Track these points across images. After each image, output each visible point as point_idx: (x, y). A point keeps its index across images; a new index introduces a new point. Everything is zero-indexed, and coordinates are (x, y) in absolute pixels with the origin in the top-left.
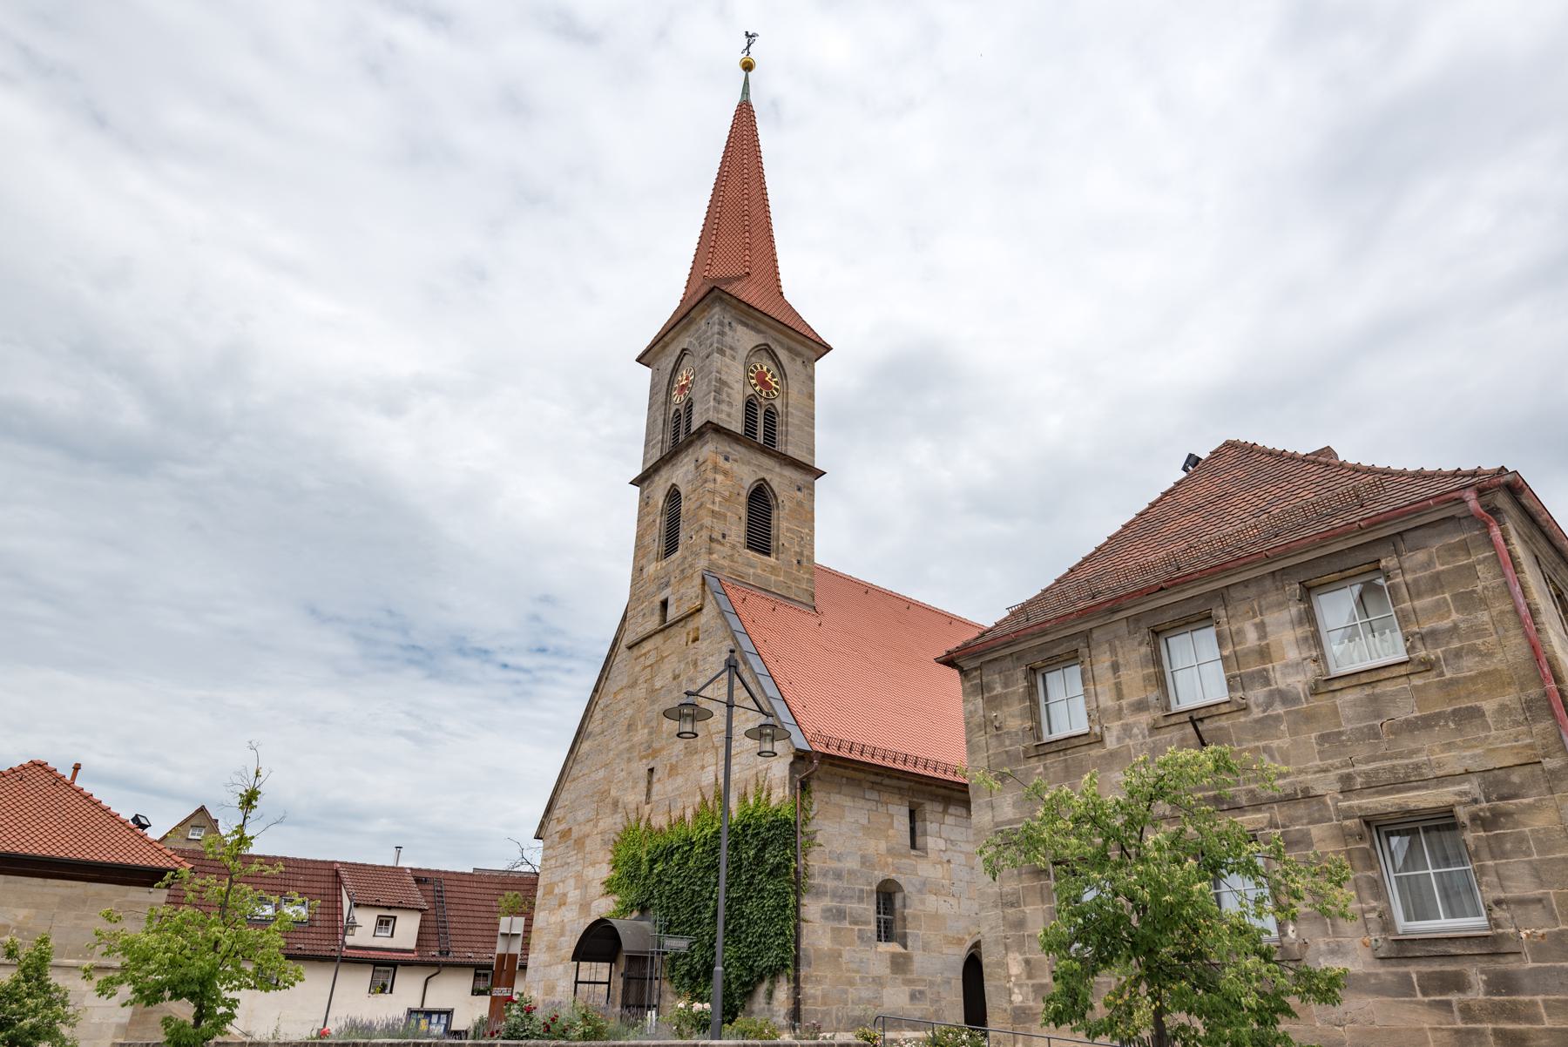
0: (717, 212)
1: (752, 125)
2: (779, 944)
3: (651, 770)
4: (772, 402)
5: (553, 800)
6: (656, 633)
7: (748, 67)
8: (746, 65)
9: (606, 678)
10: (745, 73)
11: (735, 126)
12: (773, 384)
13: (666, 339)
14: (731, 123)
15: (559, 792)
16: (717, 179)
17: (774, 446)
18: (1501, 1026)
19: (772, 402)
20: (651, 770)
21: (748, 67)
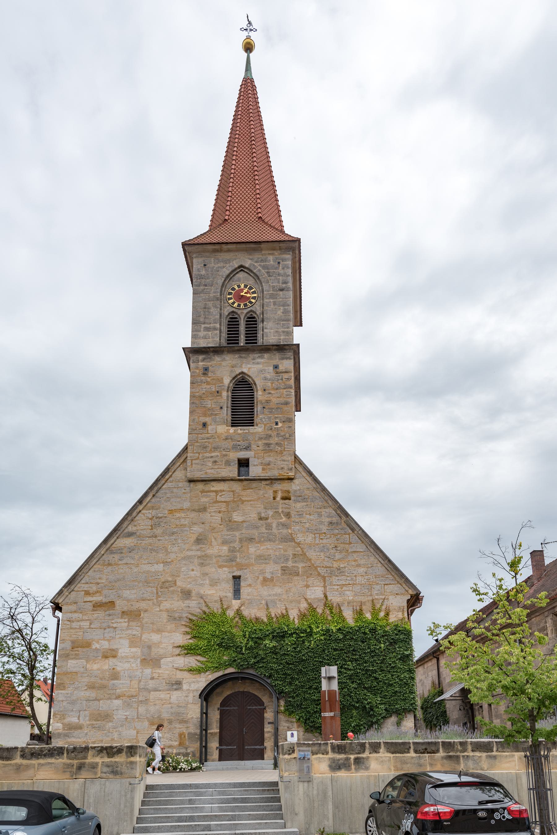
0: (227, 210)
1: (254, 94)
2: (290, 701)
3: (237, 579)
4: (251, 308)
5: (74, 578)
6: (232, 480)
7: (249, 48)
8: (248, 46)
9: (154, 496)
10: (246, 54)
11: (241, 101)
12: (248, 295)
13: (224, 246)
14: (238, 96)
15: (84, 570)
16: (232, 129)
17: (256, 343)
18: (352, 762)
19: (251, 308)
20: (237, 579)
21: (249, 48)
